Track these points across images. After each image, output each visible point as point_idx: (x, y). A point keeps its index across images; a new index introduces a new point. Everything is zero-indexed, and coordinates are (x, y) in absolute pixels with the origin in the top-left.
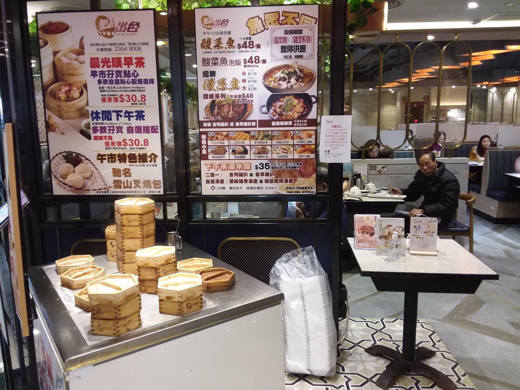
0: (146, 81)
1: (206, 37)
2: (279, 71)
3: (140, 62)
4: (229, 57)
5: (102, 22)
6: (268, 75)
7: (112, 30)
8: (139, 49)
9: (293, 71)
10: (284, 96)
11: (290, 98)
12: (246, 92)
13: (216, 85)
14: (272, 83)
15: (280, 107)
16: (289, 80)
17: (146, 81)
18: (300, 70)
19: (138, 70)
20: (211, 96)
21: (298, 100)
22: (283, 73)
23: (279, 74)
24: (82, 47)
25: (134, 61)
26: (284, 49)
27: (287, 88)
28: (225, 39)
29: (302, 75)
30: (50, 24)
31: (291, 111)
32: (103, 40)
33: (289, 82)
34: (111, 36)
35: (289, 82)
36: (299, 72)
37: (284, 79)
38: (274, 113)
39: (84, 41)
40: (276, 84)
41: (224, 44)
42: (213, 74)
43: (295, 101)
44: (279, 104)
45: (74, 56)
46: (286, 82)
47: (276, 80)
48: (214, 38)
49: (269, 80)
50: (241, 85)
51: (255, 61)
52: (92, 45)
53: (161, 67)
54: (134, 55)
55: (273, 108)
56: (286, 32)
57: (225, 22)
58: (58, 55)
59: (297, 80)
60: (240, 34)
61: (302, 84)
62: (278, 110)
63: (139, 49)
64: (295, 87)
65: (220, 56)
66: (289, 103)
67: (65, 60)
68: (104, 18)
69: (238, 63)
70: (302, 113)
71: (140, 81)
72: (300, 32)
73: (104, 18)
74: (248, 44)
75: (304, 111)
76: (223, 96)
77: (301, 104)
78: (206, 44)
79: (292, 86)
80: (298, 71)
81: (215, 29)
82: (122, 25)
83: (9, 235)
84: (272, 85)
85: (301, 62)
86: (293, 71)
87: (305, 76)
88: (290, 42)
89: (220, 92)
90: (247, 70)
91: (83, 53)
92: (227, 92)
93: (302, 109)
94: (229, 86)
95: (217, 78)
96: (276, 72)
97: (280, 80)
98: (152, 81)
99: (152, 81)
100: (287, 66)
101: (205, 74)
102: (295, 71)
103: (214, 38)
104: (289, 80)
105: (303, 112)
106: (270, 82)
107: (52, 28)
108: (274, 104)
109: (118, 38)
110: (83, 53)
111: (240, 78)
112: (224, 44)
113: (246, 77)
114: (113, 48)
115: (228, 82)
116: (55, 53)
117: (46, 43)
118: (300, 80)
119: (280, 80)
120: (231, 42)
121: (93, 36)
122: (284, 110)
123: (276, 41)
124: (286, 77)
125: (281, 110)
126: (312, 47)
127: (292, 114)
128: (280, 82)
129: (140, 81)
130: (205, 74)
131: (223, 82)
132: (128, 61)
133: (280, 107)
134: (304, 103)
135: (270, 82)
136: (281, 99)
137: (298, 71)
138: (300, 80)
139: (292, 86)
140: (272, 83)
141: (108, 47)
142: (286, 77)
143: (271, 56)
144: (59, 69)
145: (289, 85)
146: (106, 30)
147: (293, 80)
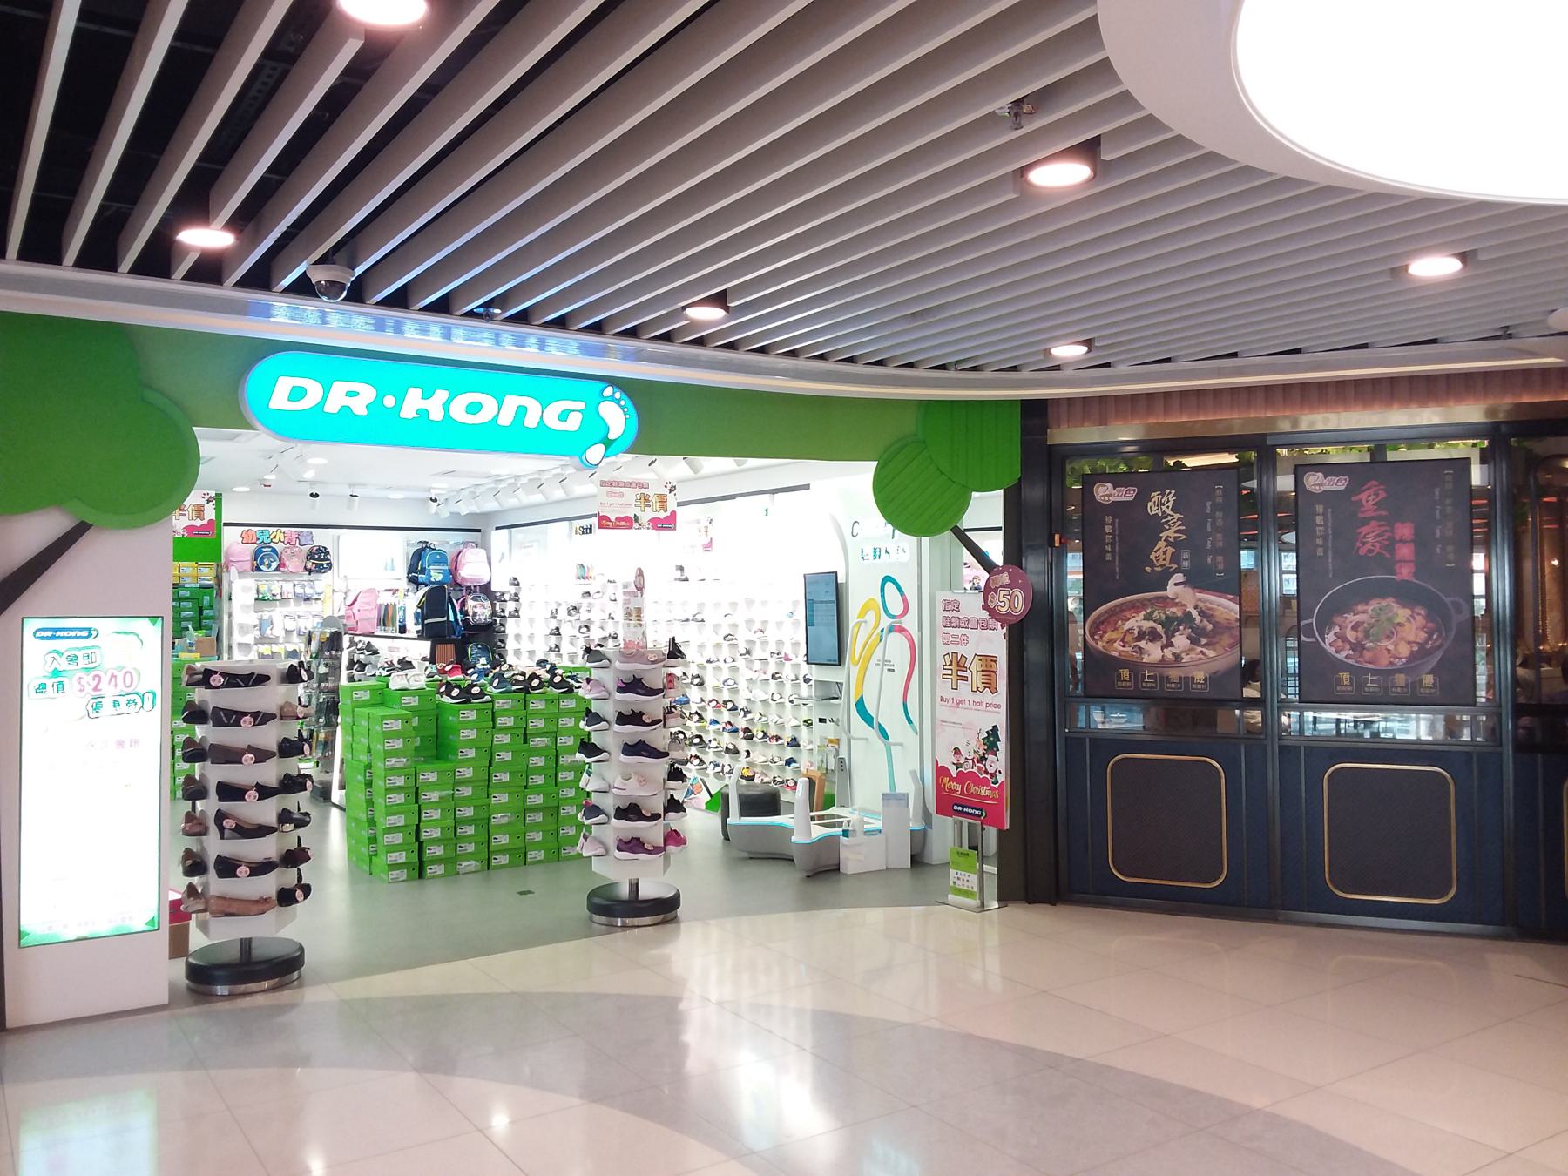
2: (1138, 613)
11: (1384, 603)
15: (1355, 628)
16: (1168, 639)
18: (1201, 613)
21: (1409, 612)
22: (1148, 618)
27: (1163, 661)
31: (1389, 637)
33: (1169, 644)
35: (1169, 644)
36: (1198, 619)
37: (1153, 636)
38: (1340, 643)
43: (1402, 614)
44: (1352, 618)
47: (1128, 638)
52: (640, 573)
55: (1337, 629)
59: (1194, 641)
61: (1211, 653)
62: (1351, 635)
64: (1186, 659)
66: (1383, 618)
70: (1422, 646)
75: (1430, 638)
77: (1420, 620)
79: (1177, 656)
80: (1195, 613)
83: (647, 920)
93: (1423, 635)
96: (1128, 614)
97: (1141, 636)
104: (1168, 639)
105: (1426, 642)
106: (1111, 641)
108: (1338, 620)
118: (1204, 641)
119: (1141, 636)
122: (1367, 635)
124: (1159, 628)
125: (1360, 635)
127: (1391, 647)
128: (1142, 644)
133: (1355, 628)
134: (1428, 618)
135: (1111, 641)
136: (1360, 608)
137: (1195, 613)
138: (1204, 641)
139: (1177, 656)
142: (1159, 628)
145: (1168, 652)
147: (1181, 641)
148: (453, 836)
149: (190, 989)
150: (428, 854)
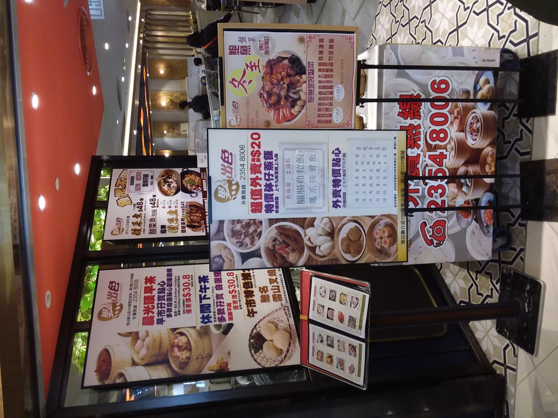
1: (130, 232)
3: (151, 280)
5: (105, 314)
6: (165, 193)
7: (114, 305)
8: (136, 281)
12: (180, 205)
13: (173, 224)
19: (157, 282)
23: (165, 188)
25: (149, 285)
26: (145, 184)
28: (135, 220)
34: (121, 306)
41: (139, 220)
42: (163, 227)
44: (189, 187)
45: (139, 342)
48: (131, 227)
50: (173, 209)
51: (153, 202)
54: (142, 285)
56: (132, 183)
57: (119, 220)
58: (137, 360)
60: (131, 211)
63: (136, 281)
65: (148, 223)
67: (143, 352)
68: (100, 313)
69: (155, 211)
71: (169, 280)
72: (132, 178)
73: (100, 313)
74: (140, 205)
76: (182, 220)
82: (110, 296)
84: (173, 191)
88: (141, 182)
89: (180, 222)
90: (161, 206)
91: (137, 333)
94: (174, 216)
95: (167, 224)
100: (159, 184)
103: (131, 227)
107: (104, 368)
110: (137, 333)
111: (168, 210)
112: (139, 220)
113: (167, 206)
114: (133, 304)
115: (171, 217)
116: (134, 364)
117: (121, 375)
120: (136, 216)
121: (120, 324)
123: (138, 189)
129: (169, 280)
130: (163, 232)
131: (171, 220)
132: (148, 290)
141: (132, 309)
143: (151, 192)
146: (114, 310)
148: (237, 190)
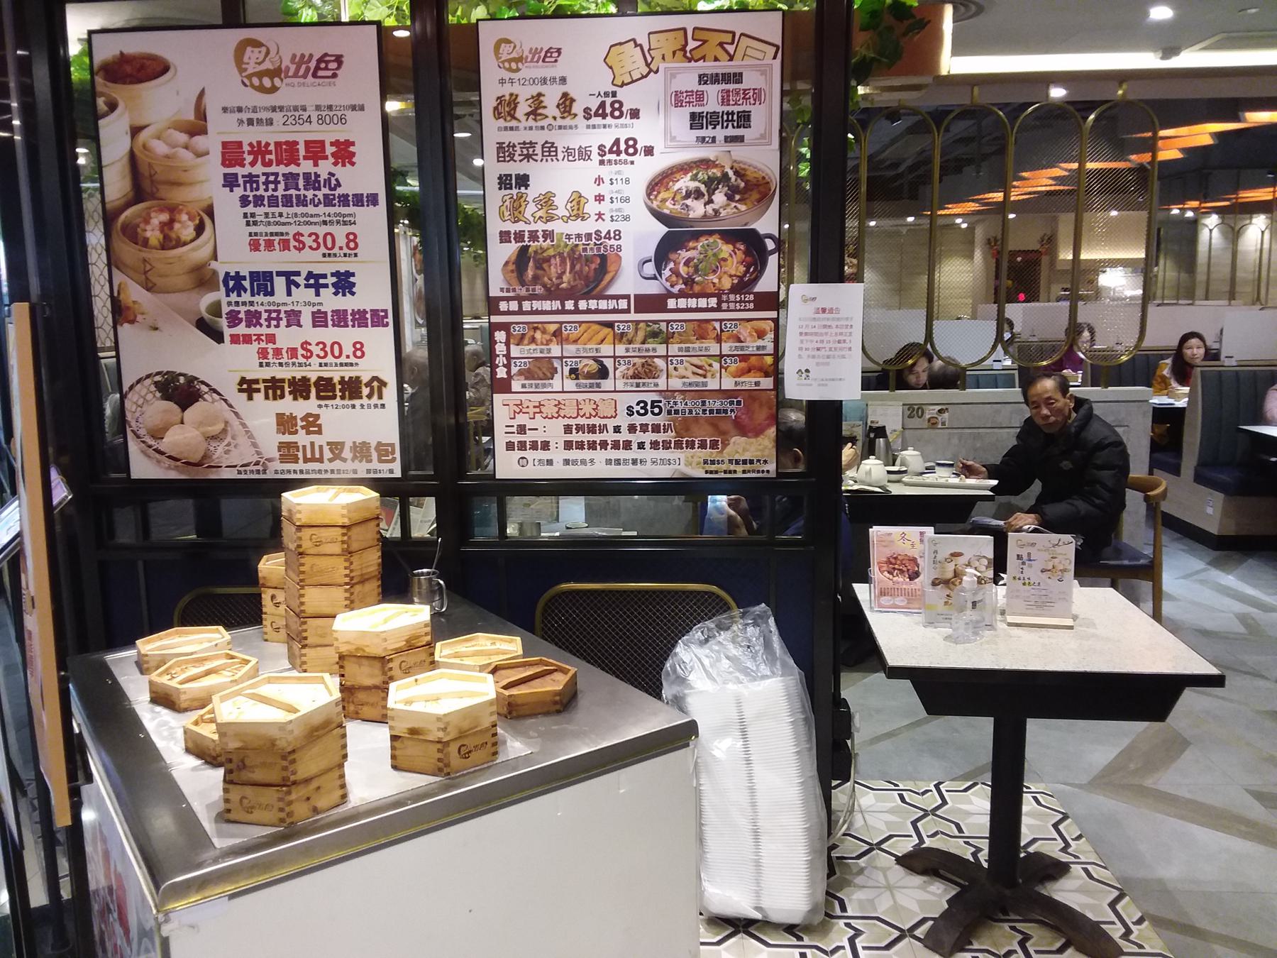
0: (358, 200)
1: (506, 90)
2: (686, 174)
3: (344, 153)
4: (563, 140)
5: (251, 55)
6: (658, 183)
7: (276, 73)
8: (342, 120)
9: (719, 174)
10: (696, 236)
11: (711, 240)
12: (604, 227)
13: (531, 209)
14: (669, 204)
15: (687, 264)
16: (710, 196)
17: (358, 200)
18: (736, 173)
19: (340, 172)
20: (519, 236)
21: (731, 247)
22: (694, 178)
23: (685, 183)
24: (201, 114)
25: (330, 150)
26: (696, 121)
27: (705, 216)
28: (552, 97)
29: (743, 185)
30: (123, 59)
31: (714, 272)
32: (252, 98)
33: (710, 201)
34: (274, 89)
35: (710, 201)
36: (733, 178)
37: (698, 194)
38: (674, 278)
39: (207, 100)
40: (678, 207)
41: (551, 109)
42: (523, 181)
43: (725, 249)
44: (684, 255)
45: (182, 138)
46: (703, 201)
47: (678, 197)
48: (525, 93)
49: (660, 197)
50: (592, 208)
51: (625, 149)
53: (395, 164)
54: (329, 134)
55: (671, 265)
56: (703, 79)
57: (552, 55)
58: (143, 136)
59: (730, 198)
60: (588, 83)
61: (743, 207)
62: (683, 270)
63: (342, 120)
64: (723, 213)
65: (539, 137)
66: (710, 253)
67: (160, 148)
68: (257, 44)
69: (584, 154)
70: (741, 278)
71: (344, 200)
72: (738, 78)
73: (257, 44)
74: (609, 108)
75: (747, 272)
76: (548, 235)
77: (740, 255)
78: (507, 108)
79: (716, 212)
80: (731, 173)
81: (527, 72)
82: (301, 61)
83: (23, 576)
84: (669, 208)
85: (738, 152)
86: (719, 174)
87: (748, 188)
88: (712, 104)
89: (540, 227)
90: (606, 172)
91: (203, 131)
92: (557, 227)
93: (742, 269)
94: (561, 211)
95: (533, 192)
96: (678, 176)
97: (688, 195)
98: (373, 200)
99: (373, 200)
100: (705, 163)
101: (504, 182)
102: (725, 175)
103: (525, 93)
104: (710, 196)
105: (745, 275)
106: (664, 201)
107: (128, 69)
108: (672, 256)
109: (289, 93)
110: (203, 131)
111: (589, 191)
112: (551, 109)
113: (604, 189)
114: (278, 117)
115: (561, 201)
116: (135, 131)
117: (112, 106)
118: (737, 197)
119: (688, 195)
120: (566, 103)
121: (227, 89)
122: (697, 270)
123: (679, 99)
124: (703, 188)
125: (691, 270)
126: (766, 116)
127: (716, 281)
128: (689, 202)
129: (344, 200)
130: (504, 182)
131: (547, 201)
132: (315, 151)
133: (687, 264)
134: (746, 253)
135: (664, 201)
136: (691, 244)
137: (731, 173)
138: (737, 197)
139: (716, 212)
140: (669, 204)
141: (264, 115)
142: (703, 188)
143: (665, 138)
144: (144, 169)
145: (710, 208)
146: (260, 75)
147: (719, 198)
149: (382, 503)
150: (113, 353)
